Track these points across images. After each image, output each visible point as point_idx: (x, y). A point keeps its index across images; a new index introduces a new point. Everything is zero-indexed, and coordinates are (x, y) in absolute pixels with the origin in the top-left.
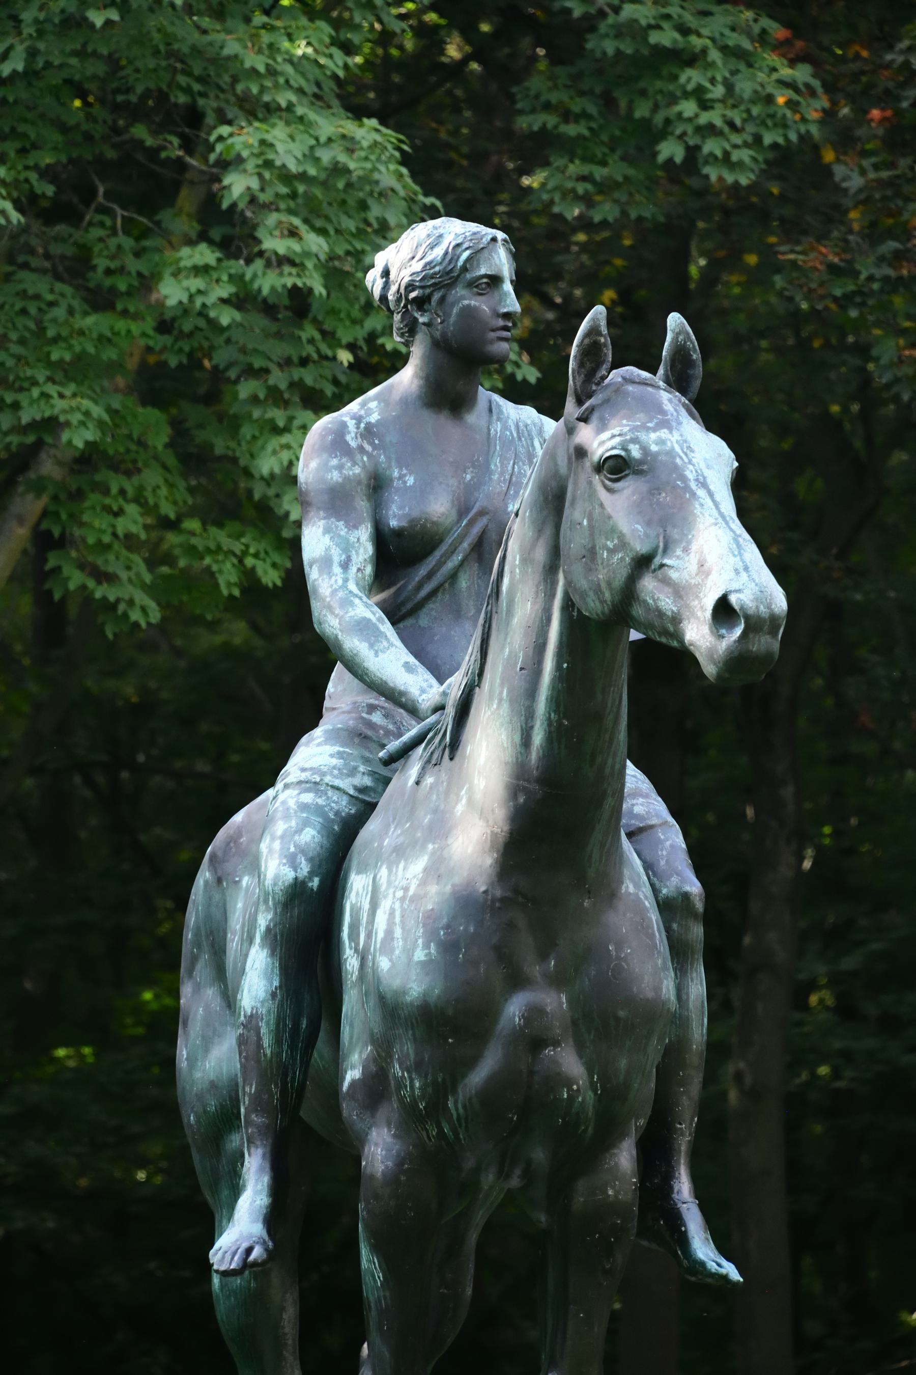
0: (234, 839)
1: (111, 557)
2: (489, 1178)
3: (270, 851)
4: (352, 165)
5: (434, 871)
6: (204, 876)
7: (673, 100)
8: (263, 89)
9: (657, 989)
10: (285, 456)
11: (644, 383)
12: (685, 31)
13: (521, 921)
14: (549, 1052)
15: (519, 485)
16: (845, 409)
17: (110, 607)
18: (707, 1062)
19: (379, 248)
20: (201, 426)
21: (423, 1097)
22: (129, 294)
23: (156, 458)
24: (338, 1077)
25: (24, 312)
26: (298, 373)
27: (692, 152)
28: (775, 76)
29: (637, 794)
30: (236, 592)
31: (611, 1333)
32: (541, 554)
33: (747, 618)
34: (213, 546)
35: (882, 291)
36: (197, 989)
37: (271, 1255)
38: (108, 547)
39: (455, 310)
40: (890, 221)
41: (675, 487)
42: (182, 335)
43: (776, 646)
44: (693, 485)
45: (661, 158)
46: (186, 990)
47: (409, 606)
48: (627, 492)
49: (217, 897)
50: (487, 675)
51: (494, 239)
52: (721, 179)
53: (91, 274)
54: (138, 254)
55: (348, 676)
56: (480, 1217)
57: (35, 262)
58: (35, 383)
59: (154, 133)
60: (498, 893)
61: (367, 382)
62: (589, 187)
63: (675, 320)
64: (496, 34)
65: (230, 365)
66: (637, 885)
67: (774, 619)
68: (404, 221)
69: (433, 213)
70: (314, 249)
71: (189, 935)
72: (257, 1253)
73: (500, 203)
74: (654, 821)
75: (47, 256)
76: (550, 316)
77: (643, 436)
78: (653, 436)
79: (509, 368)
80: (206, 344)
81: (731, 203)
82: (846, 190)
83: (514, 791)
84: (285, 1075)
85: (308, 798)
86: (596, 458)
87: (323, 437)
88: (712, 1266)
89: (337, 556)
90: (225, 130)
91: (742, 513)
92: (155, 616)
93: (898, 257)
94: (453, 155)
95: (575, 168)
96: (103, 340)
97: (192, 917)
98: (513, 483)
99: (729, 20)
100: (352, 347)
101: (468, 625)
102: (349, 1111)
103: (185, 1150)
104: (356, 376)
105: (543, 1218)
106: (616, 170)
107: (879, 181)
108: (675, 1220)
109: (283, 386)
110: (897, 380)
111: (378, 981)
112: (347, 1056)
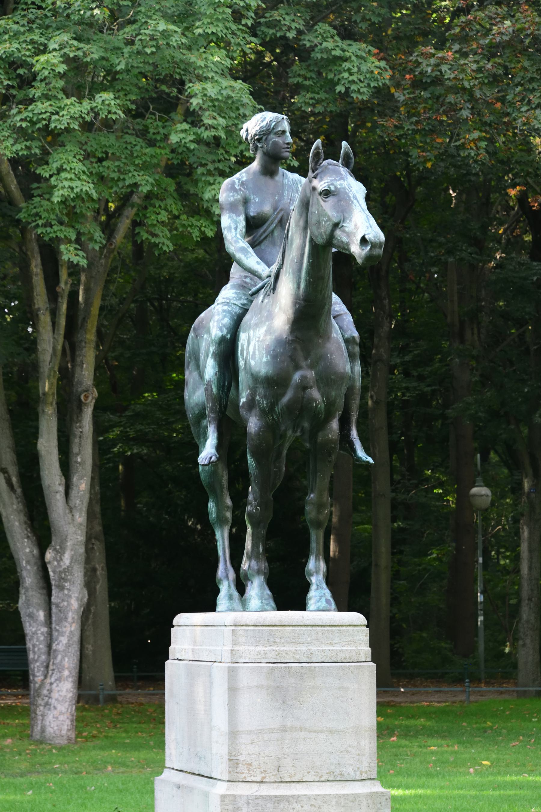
0: (201, 322)
1: (157, 228)
2: (290, 433)
3: (213, 326)
4: (233, 95)
5: (269, 331)
6: (191, 335)
7: (340, 73)
8: (203, 72)
9: (345, 369)
10: (213, 192)
11: (335, 165)
12: (343, 51)
13: (298, 347)
14: (309, 391)
15: (294, 200)
16: (402, 174)
17: (156, 245)
18: (362, 393)
19: (243, 123)
20: (186, 184)
21: (267, 407)
22: (161, 141)
23: (171, 195)
24: (238, 401)
25: (126, 148)
26: (217, 165)
27: (347, 89)
28: (374, 65)
29: (336, 303)
30: (199, 239)
31: (331, 482)
32: (302, 223)
33: (372, 243)
34: (190, 224)
35: (412, 133)
36: (191, 373)
37: (218, 459)
38: (156, 225)
39: (271, 142)
40: (414, 111)
41: (346, 199)
42: (178, 154)
43: (381, 252)
44: (352, 199)
45: (337, 91)
46: (187, 373)
47: (258, 242)
48: (330, 202)
49: (196, 342)
50: (285, 265)
51: (283, 118)
52: (357, 98)
53: (148, 135)
54: (163, 128)
55: (238, 266)
56: (287, 445)
57: (130, 132)
58: (130, 172)
59: (168, 88)
60: (290, 338)
61: (241, 168)
62: (314, 101)
63: (344, 144)
64: (282, 52)
65: (194, 163)
66: (337, 334)
67: (380, 243)
68: (252, 114)
69: (261, 111)
70: (221, 123)
71: (187, 355)
72: (214, 459)
73: (285, 107)
74: (342, 313)
75: (134, 129)
76: (302, 144)
77: (335, 183)
78: (338, 183)
79: (288, 162)
80: (186, 156)
81: (361, 106)
82: (399, 101)
83: (295, 303)
84: (221, 400)
85: (226, 308)
86: (319, 190)
87: (227, 186)
88: (364, 459)
89: (233, 226)
90: (191, 85)
91: (369, 209)
92: (172, 248)
93: (417, 122)
94: (268, 92)
95: (309, 95)
96: (152, 156)
97: (188, 349)
98: (292, 200)
99: (358, 47)
100: (236, 156)
101: (278, 248)
102: (242, 412)
103: (188, 427)
104: (237, 166)
105: (308, 445)
106: (322, 95)
107: (410, 98)
108: (351, 444)
109: (212, 169)
110: (418, 163)
111: (251, 368)
112: (241, 394)
